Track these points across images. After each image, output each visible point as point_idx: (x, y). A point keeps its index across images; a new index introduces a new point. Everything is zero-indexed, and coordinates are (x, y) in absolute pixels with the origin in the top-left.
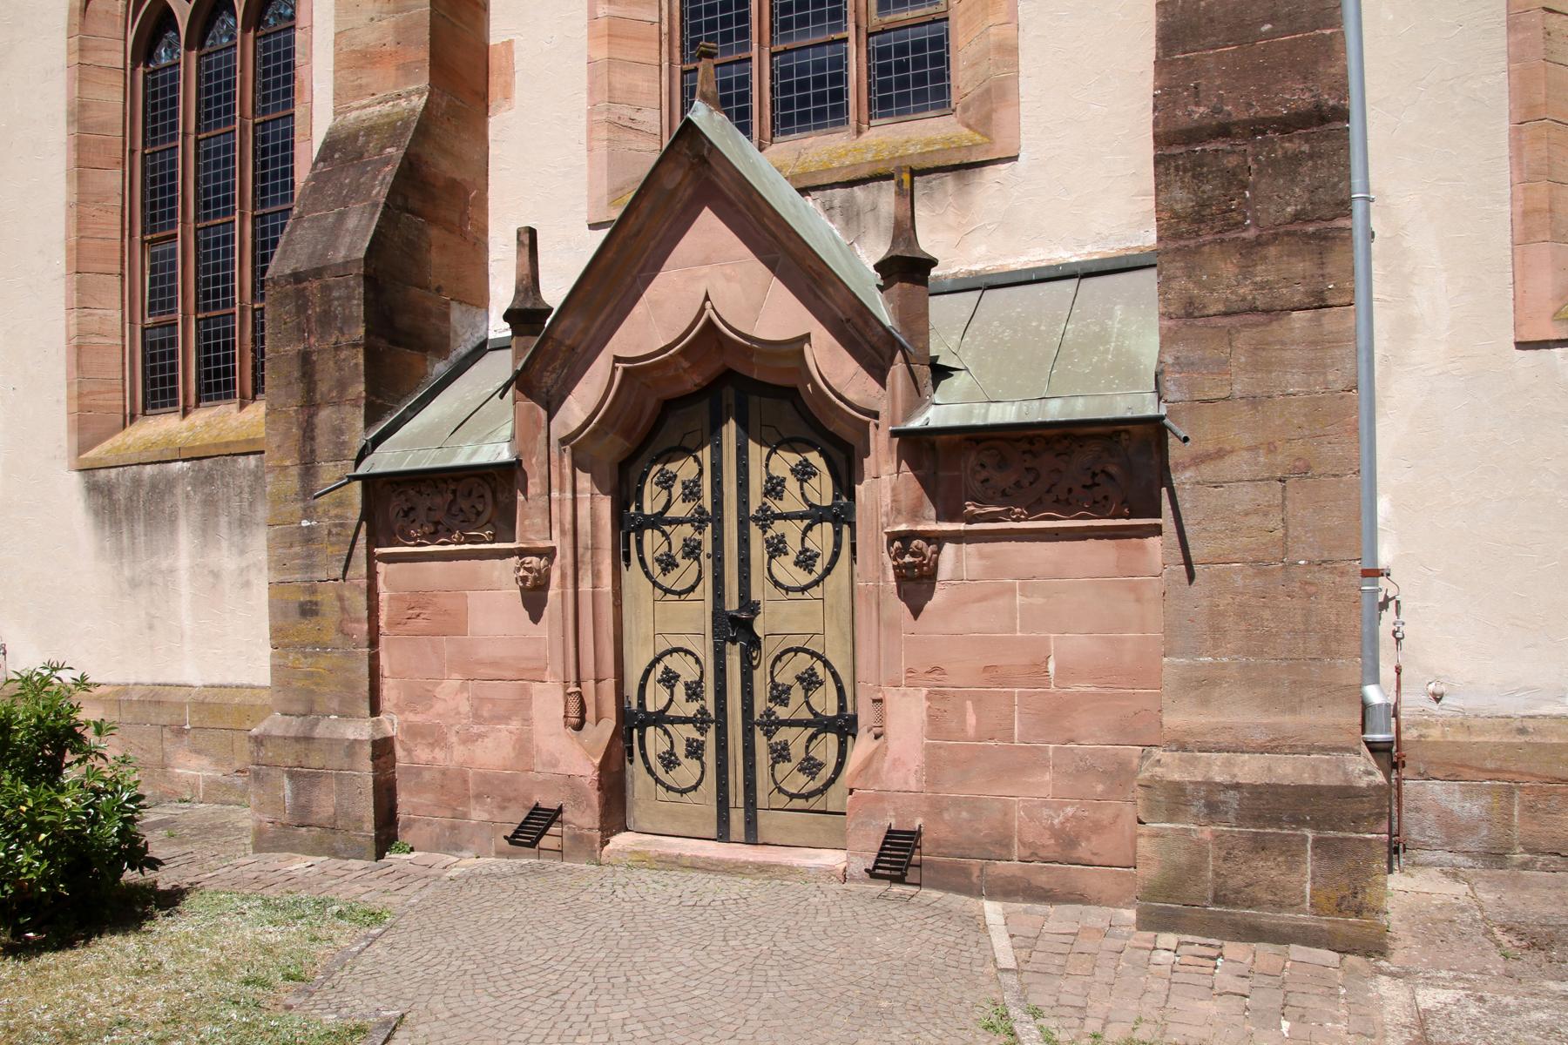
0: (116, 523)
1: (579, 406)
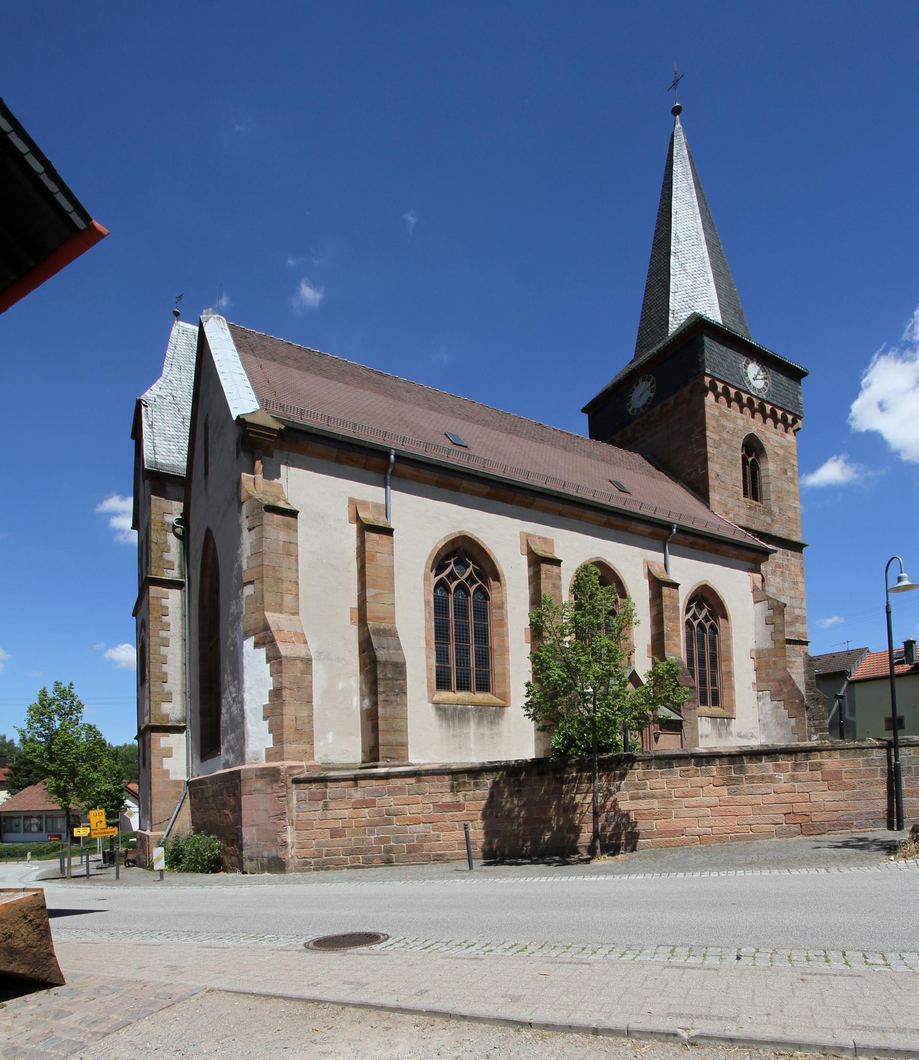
0: (447, 719)
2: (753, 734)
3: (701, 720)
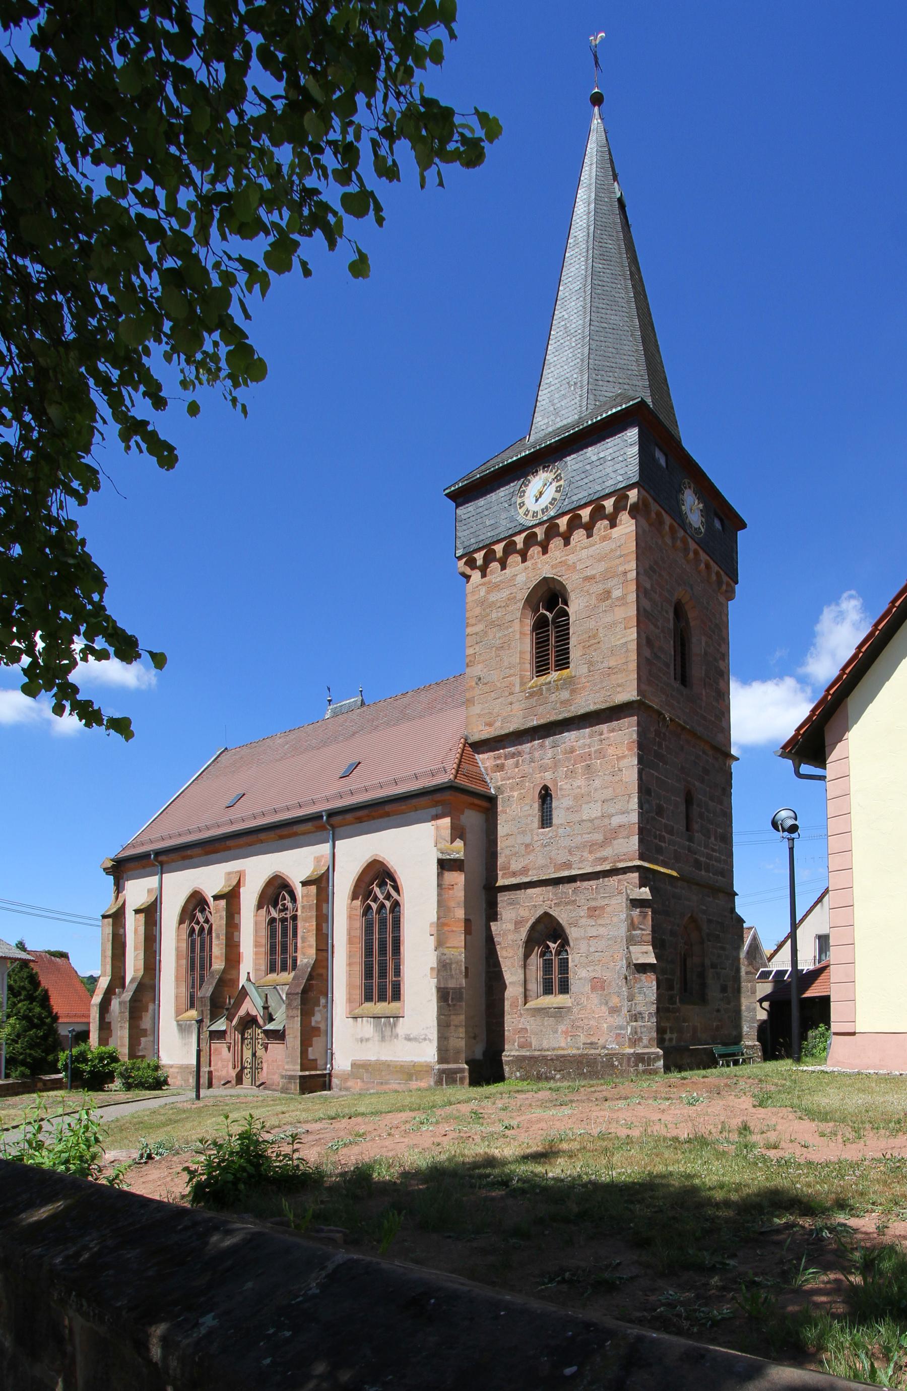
1: (234, 1022)
2: (426, 1035)
3: (362, 1021)
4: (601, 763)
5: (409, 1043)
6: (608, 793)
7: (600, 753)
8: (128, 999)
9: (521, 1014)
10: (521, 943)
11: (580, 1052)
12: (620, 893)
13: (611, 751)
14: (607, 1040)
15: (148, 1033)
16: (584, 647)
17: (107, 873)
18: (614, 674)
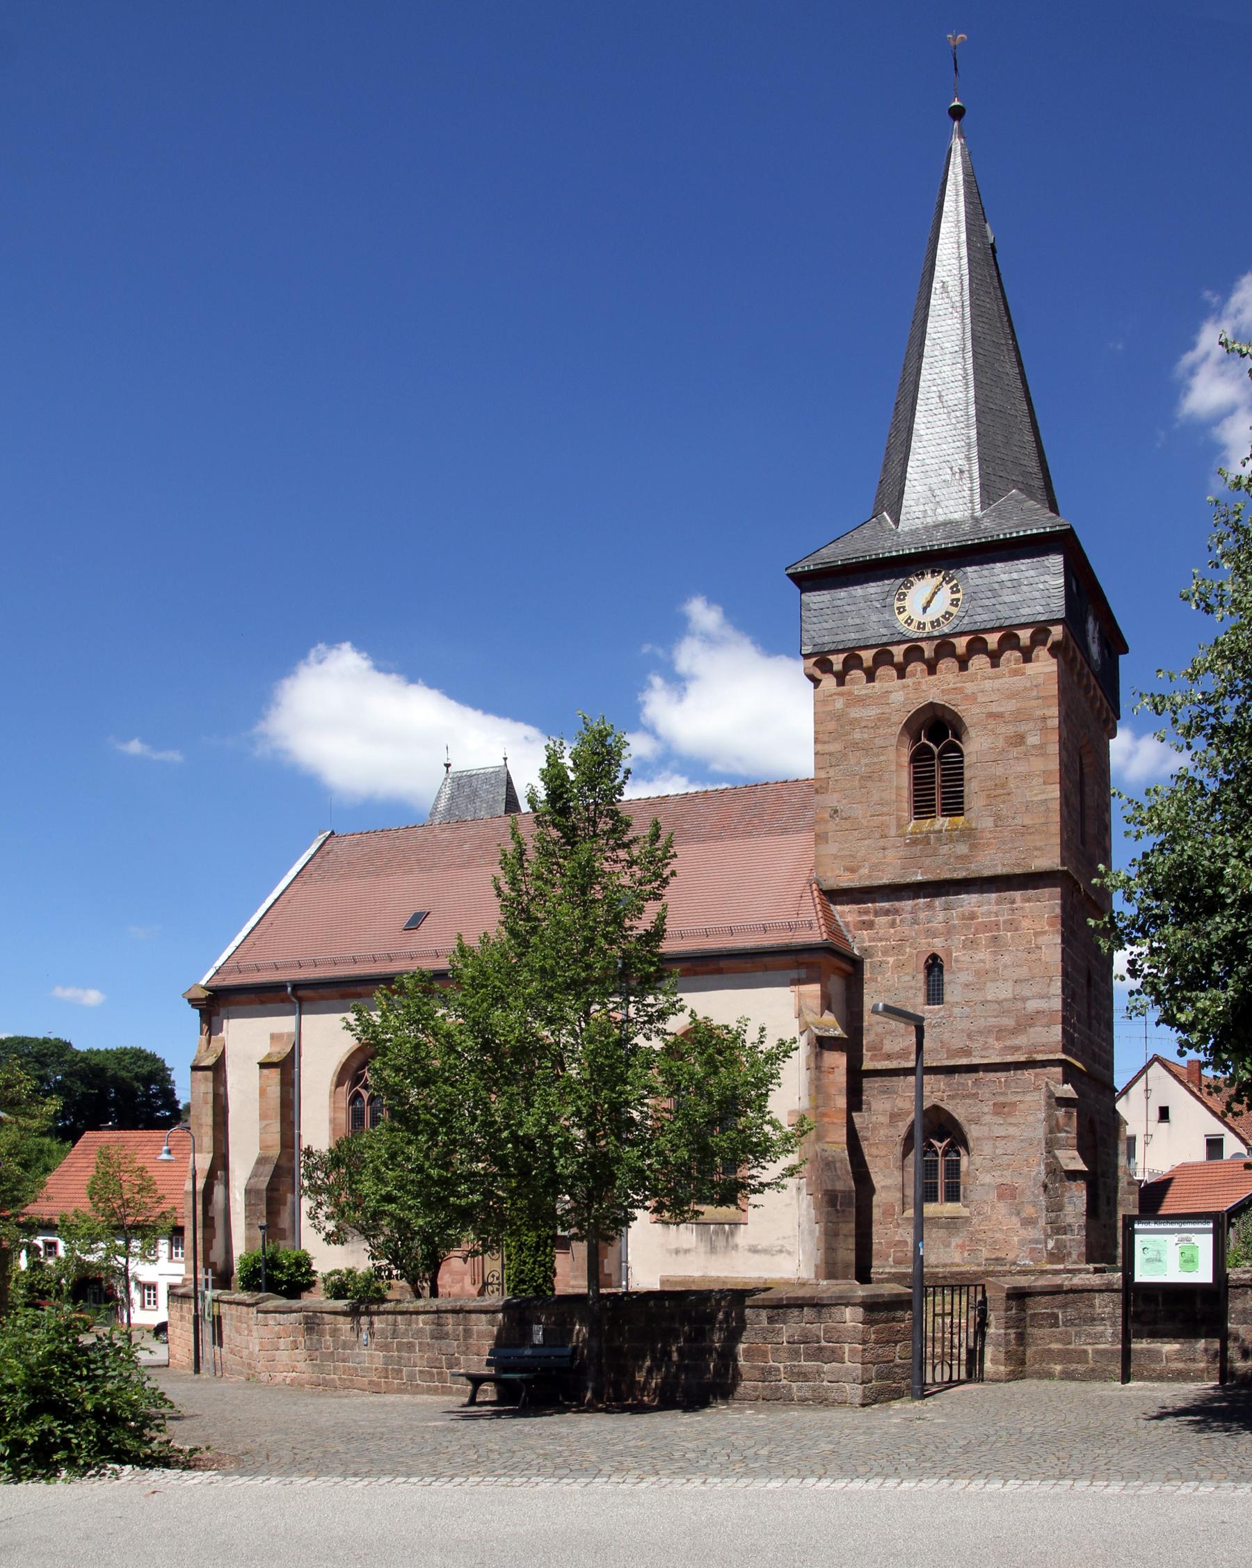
2: (783, 1246)
4: (1012, 937)
5: (756, 1256)
6: (1023, 972)
7: (1012, 925)
8: (264, 1186)
9: (898, 1224)
10: (898, 1140)
11: (982, 1268)
12: (1037, 1089)
13: (1025, 923)
14: (1018, 1256)
15: (287, 1234)
16: (988, 796)
17: (193, 1006)
18: (1030, 834)
